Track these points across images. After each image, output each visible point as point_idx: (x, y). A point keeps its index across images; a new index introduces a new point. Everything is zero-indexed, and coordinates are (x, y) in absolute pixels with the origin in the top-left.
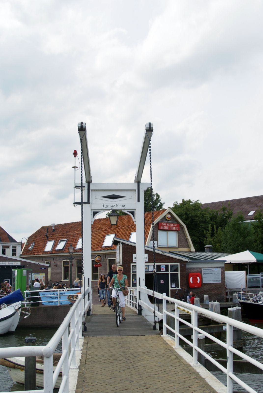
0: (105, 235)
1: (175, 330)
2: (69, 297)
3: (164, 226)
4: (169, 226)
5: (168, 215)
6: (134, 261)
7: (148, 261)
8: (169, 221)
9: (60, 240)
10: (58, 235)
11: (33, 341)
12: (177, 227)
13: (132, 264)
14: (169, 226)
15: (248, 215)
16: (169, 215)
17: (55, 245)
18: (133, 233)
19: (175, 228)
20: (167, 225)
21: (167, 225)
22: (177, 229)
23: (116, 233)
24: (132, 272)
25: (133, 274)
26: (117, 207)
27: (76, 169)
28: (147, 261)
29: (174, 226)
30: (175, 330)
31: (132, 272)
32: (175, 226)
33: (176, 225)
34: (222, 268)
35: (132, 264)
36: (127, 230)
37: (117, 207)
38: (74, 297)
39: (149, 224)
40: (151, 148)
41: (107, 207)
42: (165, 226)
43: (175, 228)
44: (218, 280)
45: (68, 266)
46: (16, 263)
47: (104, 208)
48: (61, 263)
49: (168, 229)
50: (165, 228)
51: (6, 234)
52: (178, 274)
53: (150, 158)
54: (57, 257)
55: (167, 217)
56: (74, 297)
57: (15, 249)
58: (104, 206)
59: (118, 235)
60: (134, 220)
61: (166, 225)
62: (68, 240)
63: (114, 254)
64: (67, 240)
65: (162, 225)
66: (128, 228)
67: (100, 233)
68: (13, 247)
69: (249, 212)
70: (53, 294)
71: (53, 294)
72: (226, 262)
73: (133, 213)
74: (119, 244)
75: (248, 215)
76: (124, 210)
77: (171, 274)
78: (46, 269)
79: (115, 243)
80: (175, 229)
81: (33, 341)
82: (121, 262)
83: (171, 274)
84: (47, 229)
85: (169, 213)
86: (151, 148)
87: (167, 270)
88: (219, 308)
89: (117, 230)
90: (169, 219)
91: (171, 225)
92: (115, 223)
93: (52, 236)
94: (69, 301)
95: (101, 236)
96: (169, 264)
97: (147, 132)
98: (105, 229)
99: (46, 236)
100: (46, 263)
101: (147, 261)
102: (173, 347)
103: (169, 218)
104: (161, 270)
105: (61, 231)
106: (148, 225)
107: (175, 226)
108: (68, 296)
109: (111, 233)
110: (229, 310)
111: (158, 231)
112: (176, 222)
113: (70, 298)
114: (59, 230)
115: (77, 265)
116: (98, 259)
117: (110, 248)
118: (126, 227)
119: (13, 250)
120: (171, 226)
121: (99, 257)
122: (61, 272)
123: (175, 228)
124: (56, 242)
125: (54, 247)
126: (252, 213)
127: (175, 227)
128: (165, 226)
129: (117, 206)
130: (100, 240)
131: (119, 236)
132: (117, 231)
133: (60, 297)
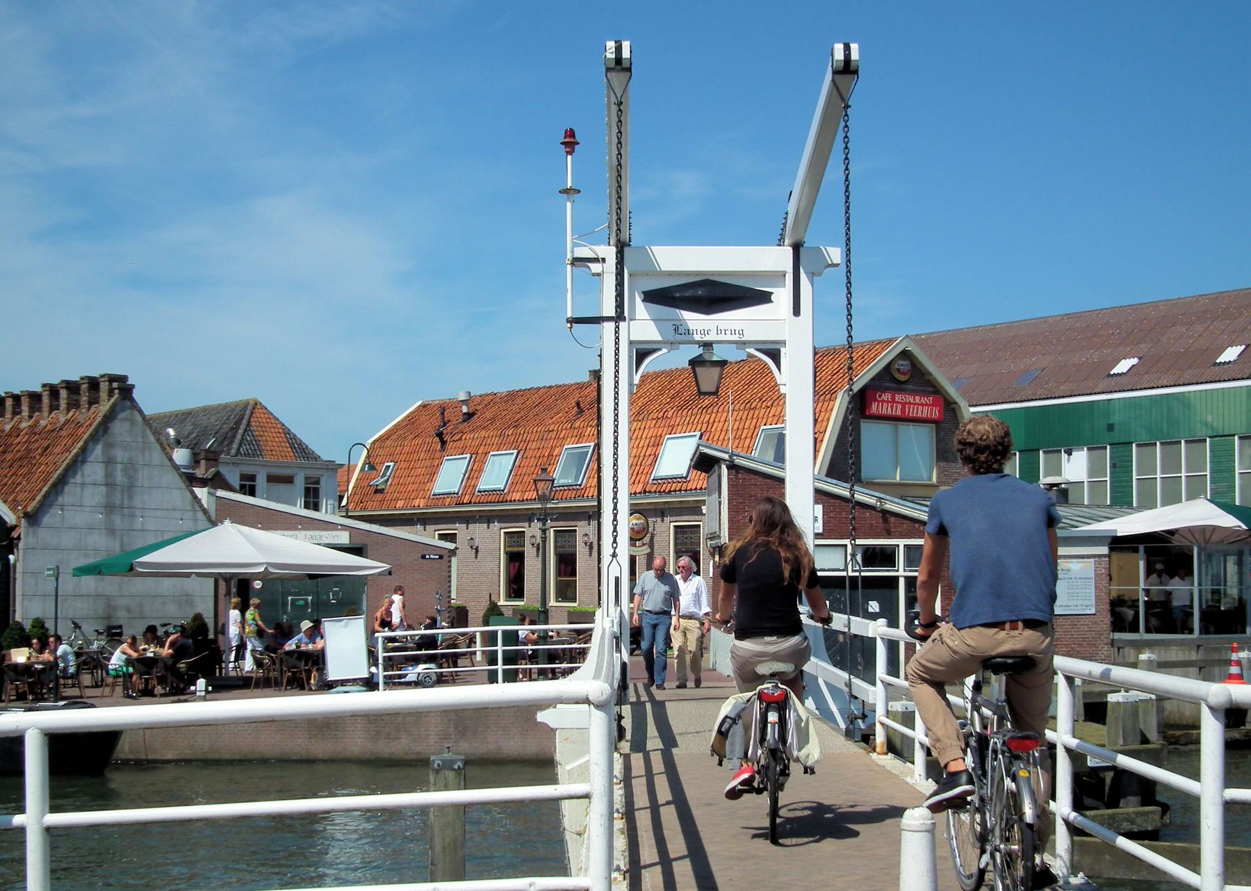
0: (661, 436)
1: (914, 730)
3: (883, 401)
4: (904, 405)
5: (901, 362)
7: (823, 529)
8: (904, 382)
9: (446, 458)
10: (483, 433)
11: (456, 767)
14: (904, 405)
15: (1218, 361)
16: (905, 363)
17: (473, 474)
18: (765, 427)
19: (925, 411)
20: (898, 397)
21: (897, 398)
22: (935, 413)
26: (719, 332)
28: (820, 530)
29: (922, 405)
30: (914, 730)
32: (926, 405)
36: (747, 418)
37: (719, 332)
39: (828, 396)
40: (848, 124)
41: (687, 333)
42: (888, 402)
43: (925, 411)
44: (1085, 603)
45: (521, 549)
46: (333, 537)
47: (679, 338)
48: (493, 538)
49: (899, 413)
50: (886, 410)
51: (279, 426)
53: (847, 158)
54: (480, 516)
55: (898, 370)
57: (314, 488)
58: (676, 330)
59: (711, 437)
60: (779, 378)
61: (893, 401)
62: (522, 452)
63: (696, 505)
64: (394, 465)
65: (876, 400)
66: (508, 435)
67: (642, 428)
68: (306, 478)
69: (1221, 350)
73: (775, 355)
74: (716, 467)
78: (446, 558)
79: (704, 463)
80: (925, 415)
81: (456, 767)
82: (722, 533)
84: (443, 413)
85: (905, 354)
86: (848, 124)
88: (1082, 704)
89: (708, 416)
90: (903, 378)
91: (912, 401)
92: (703, 389)
93: (461, 439)
95: (648, 441)
97: (836, 76)
98: (661, 414)
99: (437, 439)
100: (440, 539)
101: (820, 530)
102: (908, 780)
103: (904, 374)
105: (493, 420)
106: (822, 397)
109: (688, 426)
110: (1111, 700)
111: (862, 420)
114: (488, 415)
115: (556, 547)
116: (636, 524)
117: (680, 485)
118: (742, 406)
119: (307, 490)
120: (910, 403)
121: (638, 519)
122: (497, 572)
123: (924, 412)
124: (475, 461)
125: (468, 478)
126: (1231, 354)
127: (926, 408)
128: (888, 402)
129: (718, 331)
130: (642, 455)
131: (715, 439)
132: (706, 420)
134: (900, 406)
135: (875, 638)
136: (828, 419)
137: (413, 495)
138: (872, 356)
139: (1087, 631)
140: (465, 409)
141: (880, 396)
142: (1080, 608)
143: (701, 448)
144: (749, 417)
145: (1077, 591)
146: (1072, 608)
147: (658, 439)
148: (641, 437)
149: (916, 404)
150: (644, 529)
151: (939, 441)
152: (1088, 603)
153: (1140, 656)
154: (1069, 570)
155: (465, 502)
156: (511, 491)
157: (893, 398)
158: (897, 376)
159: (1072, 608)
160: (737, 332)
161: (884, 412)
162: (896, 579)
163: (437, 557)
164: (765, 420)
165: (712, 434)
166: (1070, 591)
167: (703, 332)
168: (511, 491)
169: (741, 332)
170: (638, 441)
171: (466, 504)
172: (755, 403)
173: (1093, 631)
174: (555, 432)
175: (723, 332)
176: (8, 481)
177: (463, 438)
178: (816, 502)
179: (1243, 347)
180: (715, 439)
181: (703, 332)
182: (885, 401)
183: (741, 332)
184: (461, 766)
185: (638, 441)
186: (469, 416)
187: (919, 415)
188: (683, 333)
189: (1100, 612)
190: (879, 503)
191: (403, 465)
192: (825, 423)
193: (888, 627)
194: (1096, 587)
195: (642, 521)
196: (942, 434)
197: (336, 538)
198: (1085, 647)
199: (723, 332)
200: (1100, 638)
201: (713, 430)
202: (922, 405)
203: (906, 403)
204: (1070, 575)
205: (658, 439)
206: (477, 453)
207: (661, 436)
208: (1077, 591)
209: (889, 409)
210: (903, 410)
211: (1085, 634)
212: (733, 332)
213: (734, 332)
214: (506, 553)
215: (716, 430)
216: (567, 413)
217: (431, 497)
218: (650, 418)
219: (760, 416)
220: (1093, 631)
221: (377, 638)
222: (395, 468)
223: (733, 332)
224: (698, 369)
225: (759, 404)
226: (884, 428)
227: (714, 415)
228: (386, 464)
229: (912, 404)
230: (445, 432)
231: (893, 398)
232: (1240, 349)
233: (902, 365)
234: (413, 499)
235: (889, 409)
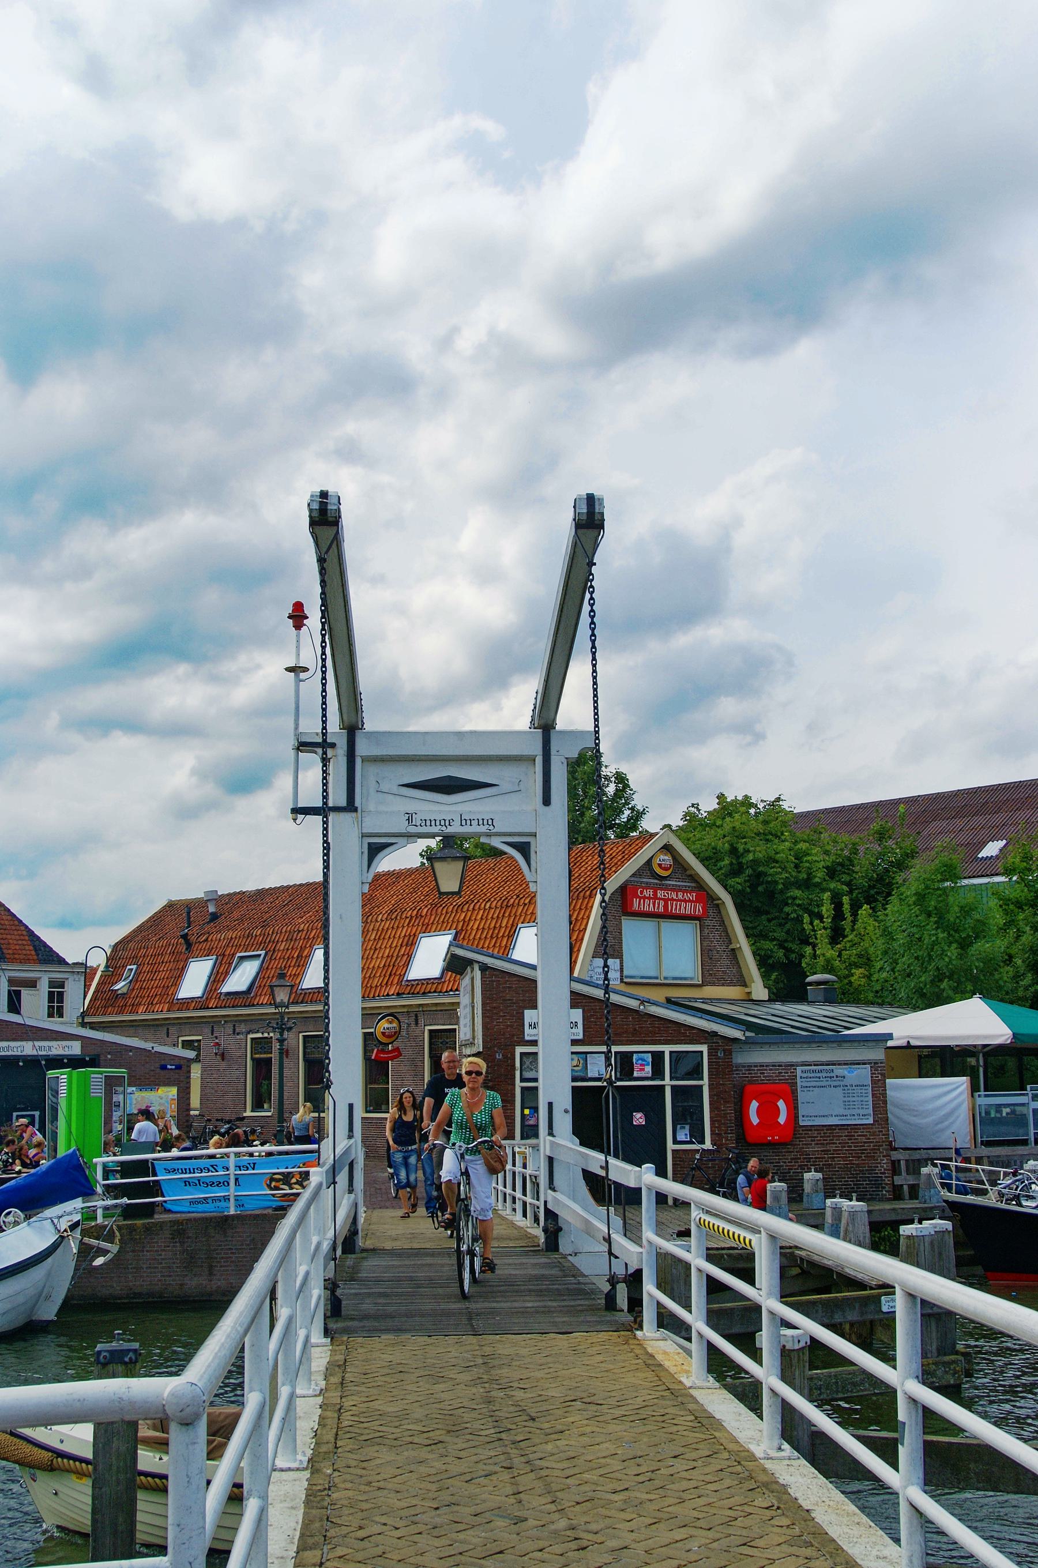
0: (414, 935)
2: (272, 1179)
3: (645, 898)
4: (666, 901)
5: (662, 857)
6: (527, 1038)
9: (239, 954)
10: (230, 934)
11: (127, 1359)
12: (696, 902)
13: (519, 1050)
15: (980, 856)
17: (218, 977)
18: (523, 925)
20: (660, 894)
23: (460, 927)
24: (522, 1080)
25: (523, 1089)
26: (464, 822)
27: (303, 676)
29: (685, 901)
31: (522, 1080)
32: (689, 901)
33: (693, 896)
34: (874, 1065)
35: (519, 1050)
36: (503, 916)
37: (464, 822)
38: (294, 1180)
42: (649, 898)
44: (862, 1112)
47: (412, 829)
49: (661, 910)
50: (648, 907)
52: (701, 1086)
54: (225, 1021)
55: (660, 865)
56: (294, 1180)
60: (528, 876)
61: (655, 897)
63: (451, 1008)
69: (983, 845)
70: (211, 1169)
71: (209, 1171)
72: (890, 1043)
73: (524, 849)
75: (980, 856)
76: (489, 835)
77: (673, 1087)
78: (184, 1068)
79: (455, 965)
80: (688, 912)
81: (127, 1359)
83: (673, 1087)
84: (189, 913)
85: (667, 848)
87: (658, 1072)
88: (867, 1223)
91: (675, 897)
93: (206, 940)
94: (273, 1195)
95: (401, 940)
96: (667, 1049)
99: (182, 941)
103: (666, 869)
104: (635, 1074)
107: (689, 901)
108: (268, 1176)
112: (693, 885)
113: (277, 1184)
114: (236, 915)
116: (388, 1029)
118: (499, 904)
119: (51, 995)
120: (673, 900)
121: (391, 1023)
122: (242, 1080)
123: (688, 909)
124: (221, 964)
128: (649, 898)
129: (463, 822)
130: (395, 955)
131: (471, 937)
132: (462, 918)
133: (237, 1179)
134: (662, 903)
135: (640, 1189)
136: (588, 917)
137: (156, 999)
138: (633, 851)
139: (865, 1142)
140: (212, 909)
141: (642, 892)
142: (856, 1117)
143: (452, 949)
144: (507, 915)
145: (854, 1099)
146: (849, 1117)
147: (411, 938)
148: (394, 937)
149: (681, 901)
150: (395, 1033)
151: (703, 939)
152: (865, 1112)
153: (922, 1169)
154: (844, 1077)
155: (210, 1006)
156: (259, 994)
157: (655, 894)
158: (658, 870)
159: (849, 1117)
160: (485, 822)
161: (646, 909)
162: (663, 1086)
163: (173, 1067)
164: (523, 918)
165: (469, 932)
166: (846, 1099)
167: (443, 823)
168: (259, 994)
169: (490, 822)
170: (391, 940)
171: (212, 1008)
172: (512, 900)
173: (871, 1142)
174: (305, 932)
175: (468, 822)
176: (578, 914)
177: (209, 939)
178: (574, 1005)
179: (1004, 842)
180: (471, 937)
181: (443, 823)
182: (647, 898)
183: (490, 822)
184: (134, 1358)
185: (391, 940)
186: (214, 917)
187: (683, 911)
188: (418, 824)
189: (877, 1121)
190: (642, 1007)
191: (146, 968)
192: (585, 921)
193: (656, 1175)
194: (873, 1095)
195: (394, 1025)
196: (706, 931)
197: (66, 1049)
198: (863, 1160)
199: (468, 822)
200: (879, 1150)
201: (469, 928)
202: (685, 901)
203: (668, 899)
204: (846, 1082)
205: (411, 938)
206: (224, 955)
207: (414, 935)
208: (854, 1099)
209: (651, 905)
210: (666, 907)
211: (863, 1146)
212: (481, 822)
213: (481, 822)
214: (252, 1059)
215: (472, 929)
216: (317, 911)
217: (175, 1002)
218: (404, 916)
219: (518, 914)
220: (871, 1142)
221: (96, 1164)
222: (139, 971)
223: (481, 822)
224: (438, 866)
225: (517, 901)
226: (648, 926)
227: (469, 913)
228: (129, 967)
229: (675, 900)
230: (190, 933)
231: (655, 894)
232: (1002, 843)
233: (663, 860)
234: (156, 1004)
235: (651, 905)
